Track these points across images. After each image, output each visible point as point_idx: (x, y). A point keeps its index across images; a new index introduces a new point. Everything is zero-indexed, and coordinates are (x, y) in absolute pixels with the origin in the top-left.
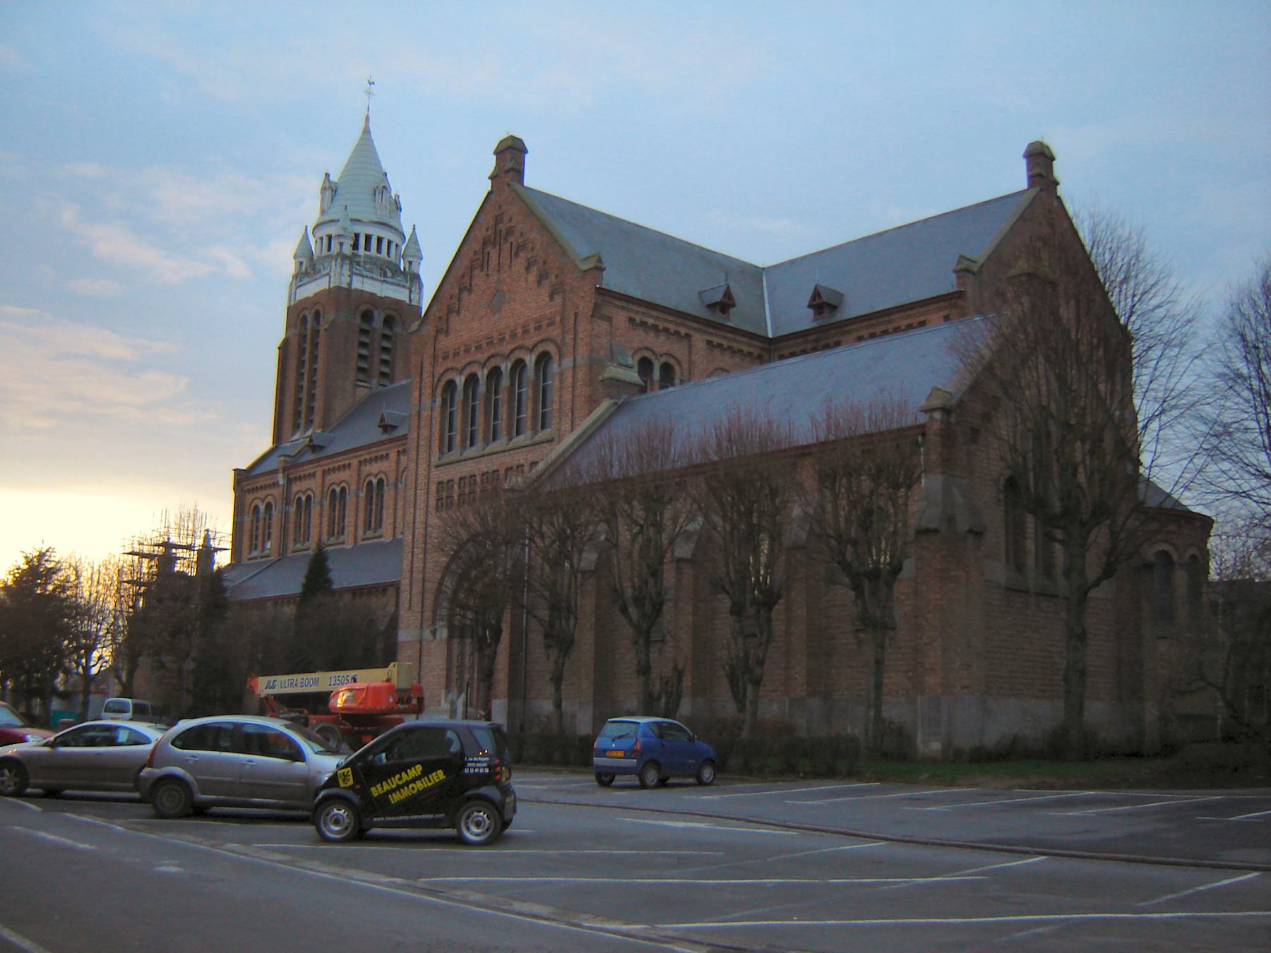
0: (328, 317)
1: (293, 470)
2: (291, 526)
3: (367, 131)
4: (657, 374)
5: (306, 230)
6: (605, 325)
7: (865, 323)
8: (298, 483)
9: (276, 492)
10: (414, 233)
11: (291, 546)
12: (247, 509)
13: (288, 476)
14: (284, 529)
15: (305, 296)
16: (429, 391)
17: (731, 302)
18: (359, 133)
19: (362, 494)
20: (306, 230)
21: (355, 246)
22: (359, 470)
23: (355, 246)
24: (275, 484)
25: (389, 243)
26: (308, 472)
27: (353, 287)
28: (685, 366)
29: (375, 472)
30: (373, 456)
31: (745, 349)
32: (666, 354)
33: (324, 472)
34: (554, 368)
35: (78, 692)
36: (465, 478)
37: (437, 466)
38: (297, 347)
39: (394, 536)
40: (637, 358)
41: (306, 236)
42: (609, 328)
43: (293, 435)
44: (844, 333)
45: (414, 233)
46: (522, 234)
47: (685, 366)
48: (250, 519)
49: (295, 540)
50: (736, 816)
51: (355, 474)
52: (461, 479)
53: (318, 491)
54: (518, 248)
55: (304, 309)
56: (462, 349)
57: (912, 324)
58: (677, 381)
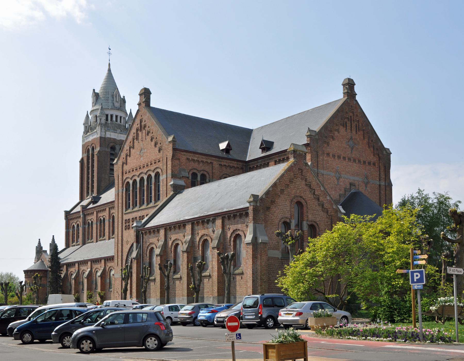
1: (86, 211)
3: (109, 70)
4: (199, 178)
5: (87, 113)
6: (177, 162)
7: (277, 155)
16: (121, 186)
17: (231, 148)
18: (106, 72)
20: (87, 113)
21: (107, 119)
23: (107, 119)
24: (80, 217)
25: (121, 117)
26: (91, 212)
27: (106, 137)
28: (211, 174)
31: (236, 166)
32: (203, 170)
34: (161, 178)
36: (141, 216)
37: (125, 214)
40: (191, 173)
41: (87, 116)
42: (179, 163)
43: (87, 197)
44: (270, 159)
46: (149, 127)
47: (211, 174)
50: (332, 349)
52: (139, 217)
53: (95, 219)
54: (148, 132)
55: (88, 146)
56: (131, 170)
58: (207, 180)
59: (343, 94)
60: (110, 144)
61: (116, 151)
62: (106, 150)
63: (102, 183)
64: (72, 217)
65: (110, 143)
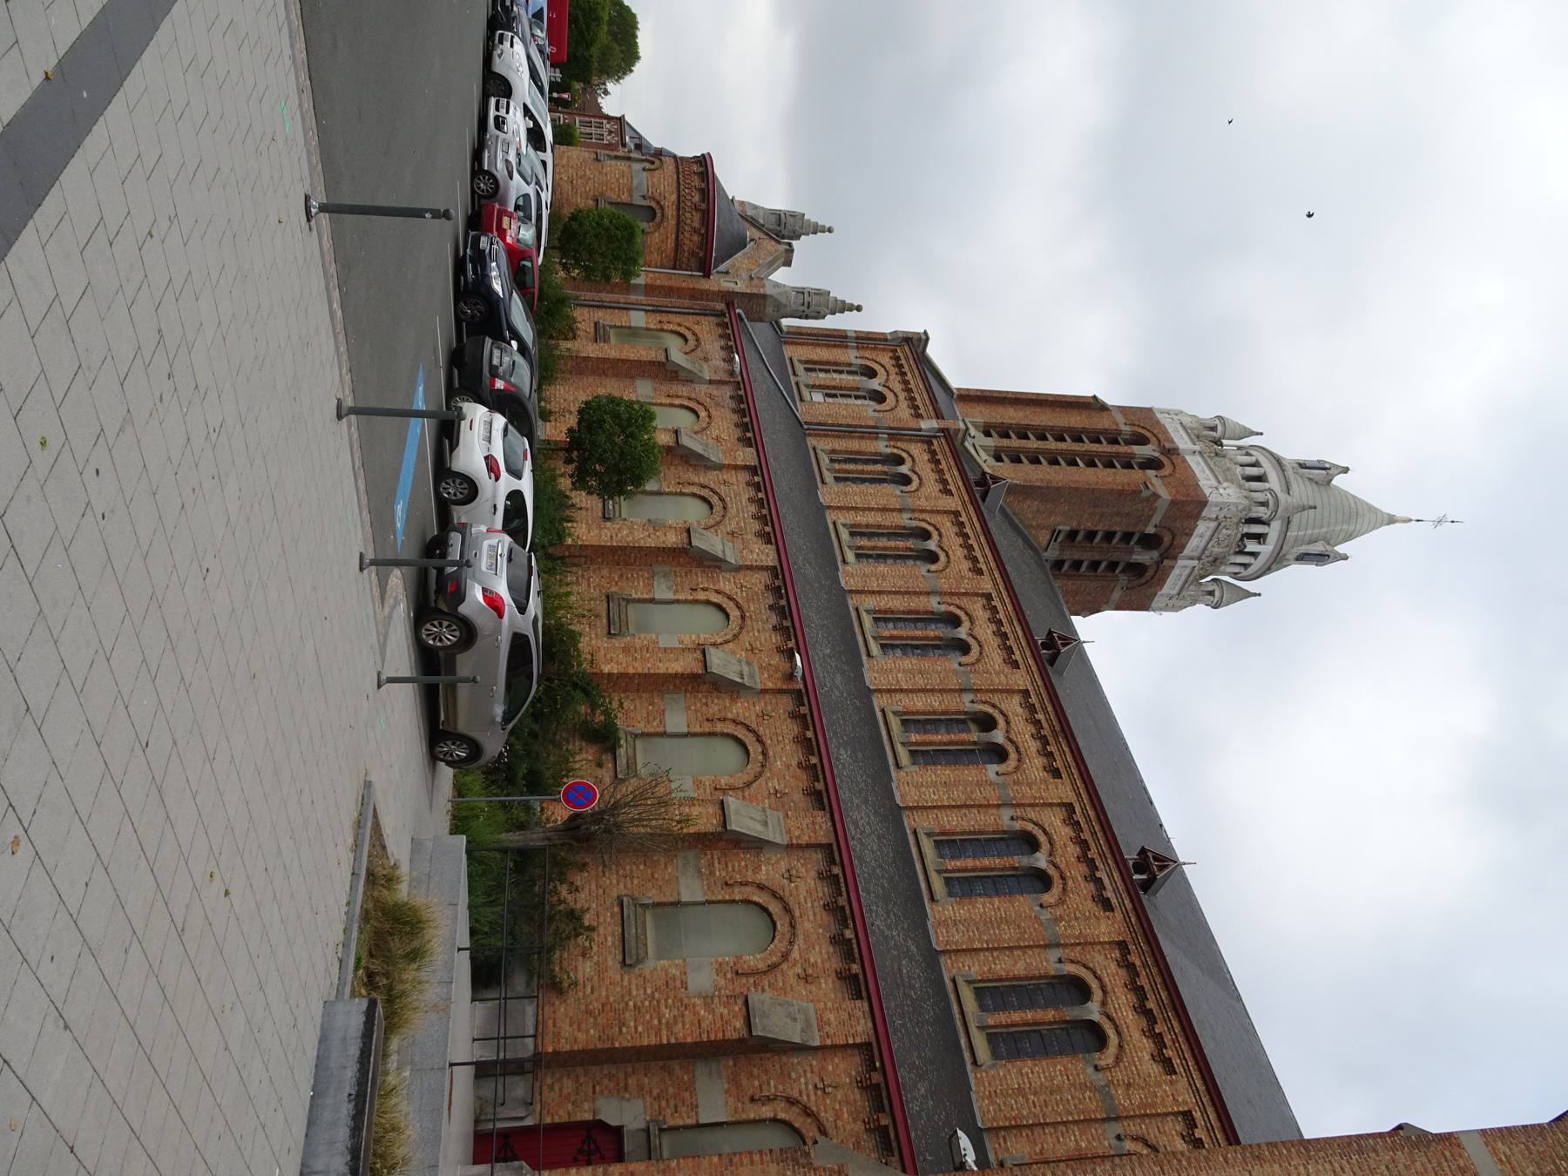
0: (1155, 481)
2: (854, 445)
3: (1392, 520)
8: (926, 457)
9: (904, 412)
10: (1248, 594)
11: (824, 444)
12: (867, 354)
13: (935, 437)
14: (848, 431)
19: (934, 604)
22: (1010, 691)
29: (978, 631)
30: (1007, 628)
33: (956, 514)
38: (1100, 426)
39: (875, 691)
45: (1248, 594)
48: (854, 361)
49: (834, 451)
51: (1000, 681)
59: (641, 54)
60: (1168, 533)
61: (1138, 549)
62: (1157, 519)
63: (1036, 503)
64: (906, 366)
65: (1173, 534)
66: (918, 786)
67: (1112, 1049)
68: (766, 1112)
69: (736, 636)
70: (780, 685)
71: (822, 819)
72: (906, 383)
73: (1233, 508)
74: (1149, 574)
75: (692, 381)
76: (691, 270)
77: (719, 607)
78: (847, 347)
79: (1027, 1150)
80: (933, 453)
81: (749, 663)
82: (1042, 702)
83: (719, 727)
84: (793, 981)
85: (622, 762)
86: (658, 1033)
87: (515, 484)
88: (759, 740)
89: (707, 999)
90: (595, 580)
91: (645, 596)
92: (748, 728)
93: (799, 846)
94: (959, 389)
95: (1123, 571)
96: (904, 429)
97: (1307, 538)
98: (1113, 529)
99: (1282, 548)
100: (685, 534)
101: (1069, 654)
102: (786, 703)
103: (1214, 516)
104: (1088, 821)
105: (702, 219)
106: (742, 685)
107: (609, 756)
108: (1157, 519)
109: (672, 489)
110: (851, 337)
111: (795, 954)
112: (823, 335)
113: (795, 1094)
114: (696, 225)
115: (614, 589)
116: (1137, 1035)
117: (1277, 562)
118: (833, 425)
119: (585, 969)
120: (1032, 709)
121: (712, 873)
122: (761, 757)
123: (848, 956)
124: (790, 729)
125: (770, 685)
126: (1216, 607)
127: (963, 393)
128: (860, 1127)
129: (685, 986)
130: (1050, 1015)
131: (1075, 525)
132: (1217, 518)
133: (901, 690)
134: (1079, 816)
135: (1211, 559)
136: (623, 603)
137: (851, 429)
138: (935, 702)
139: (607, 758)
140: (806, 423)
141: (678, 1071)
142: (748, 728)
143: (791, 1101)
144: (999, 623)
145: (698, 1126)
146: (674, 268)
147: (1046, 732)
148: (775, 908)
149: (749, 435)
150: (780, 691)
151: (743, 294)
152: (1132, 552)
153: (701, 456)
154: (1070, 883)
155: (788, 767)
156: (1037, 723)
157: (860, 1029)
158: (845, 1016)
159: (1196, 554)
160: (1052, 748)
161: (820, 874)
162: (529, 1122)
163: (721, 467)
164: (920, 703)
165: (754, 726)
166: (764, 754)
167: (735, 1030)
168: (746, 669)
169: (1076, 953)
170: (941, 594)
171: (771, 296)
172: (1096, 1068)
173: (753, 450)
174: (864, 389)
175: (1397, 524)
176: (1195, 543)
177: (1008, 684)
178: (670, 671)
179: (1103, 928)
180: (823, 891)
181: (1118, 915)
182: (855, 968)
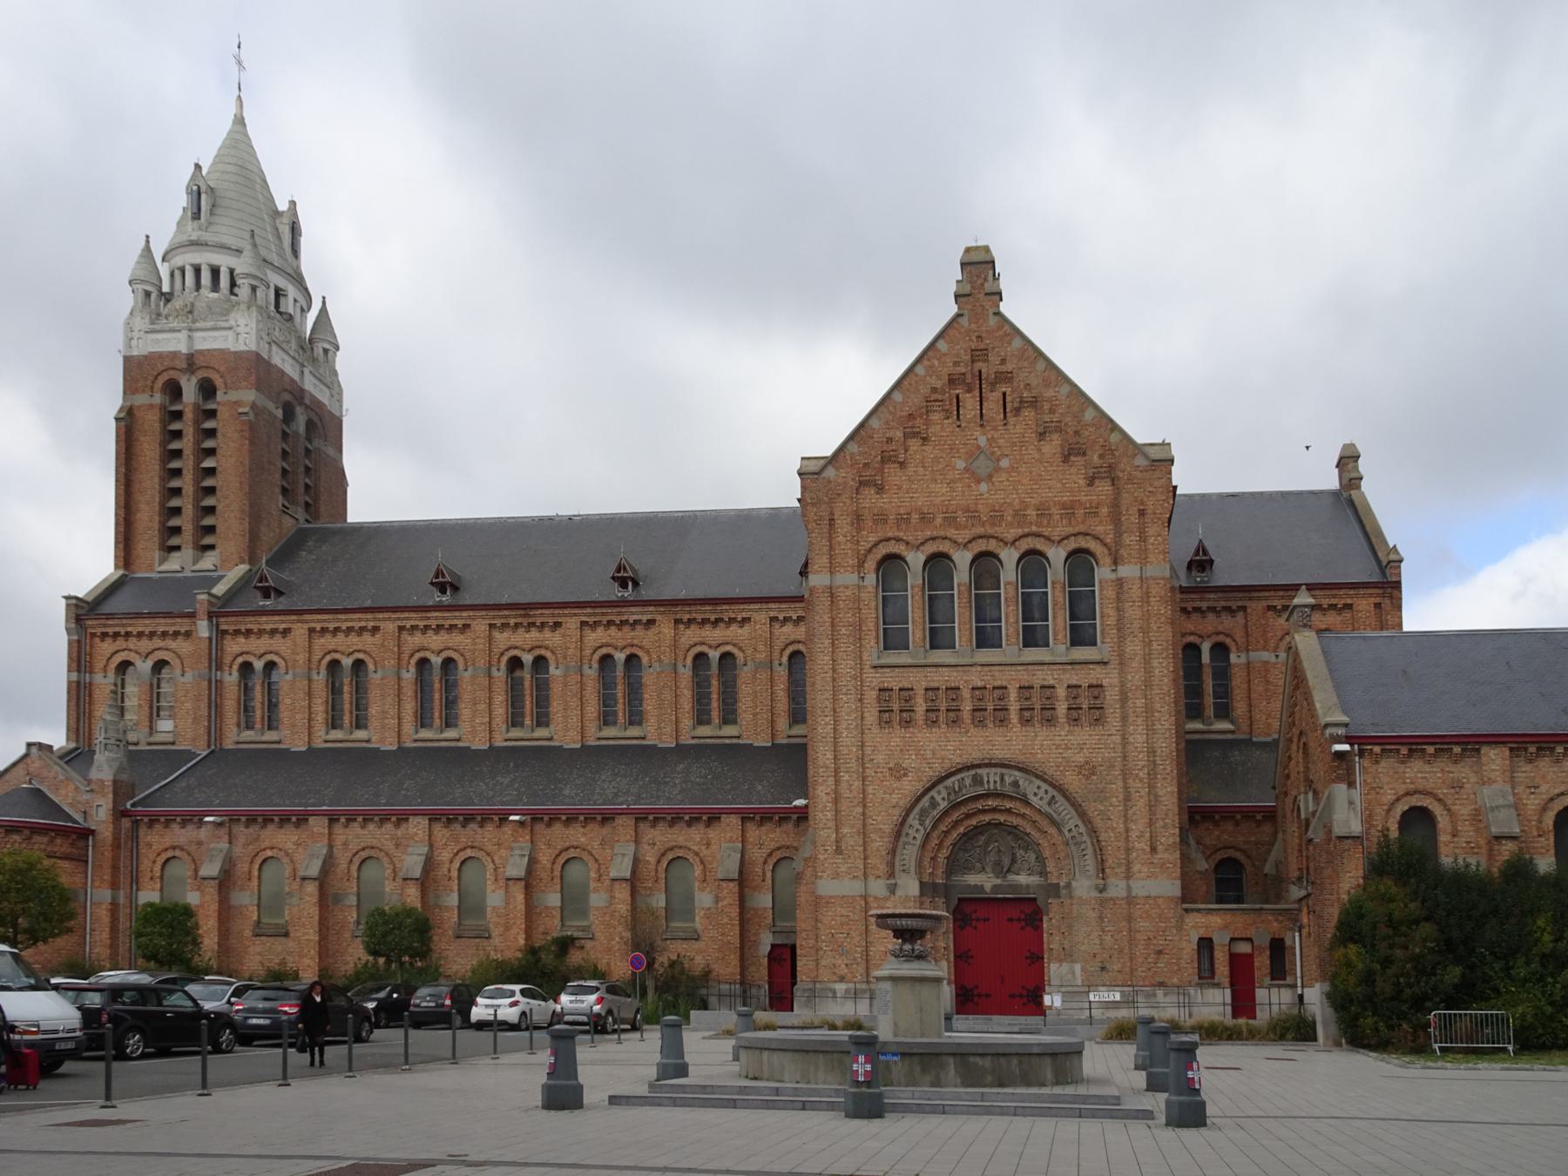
3: (240, 121)
13: (217, 625)
15: (172, 349)
18: (227, 124)
22: (490, 639)
34: (1103, 573)
35: (1043, 873)
45: (324, 311)
51: (482, 644)
57: (1336, 605)
62: (271, 406)
66: (567, 729)
67: (735, 651)
68: (769, 874)
69: (488, 854)
70: (528, 831)
71: (620, 820)
72: (140, 635)
73: (261, 325)
74: (315, 419)
75: (231, 858)
76: (88, 846)
77: (463, 863)
78: (90, 684)
79: (783, 720)
80: (237, 632)
81: (512, 849)
82: (501, 617)
83: (557, 873)
84: (709, 852)
85: (580, 934)
86: (733, 925)
87: (518, 993)
88: (567, 849)
89: (717, 899)
90: (443, 946)
91: (456, 912)
92: (558, 855)
93: (636, 836)
94: (117, 567)
95: (311, 442)
96: (210, 653)
97: (277, 242)
98: (280, 451)
99: (289, 274)
100: (409, 882)
101: (452, 573)
102: (539, 827)
103: (267, 346)
104: (594, 614)
105: (40, 834)
106: (530, 855)
107: (576, 941)
108: (271, 406)
109: (355, 885)
110: (79, 677)
111: (696, 848)
112: (78, 706)
113: (762, 859)
114: (45, 839)
115: (450, 933)
116: (728, 632)
117: (298, 280)
118: (209, 721)
119: (699, 959)
120: (505, 626)
121: (650, 888)
122: (578, 850)
123: (698, 819)
124: (558, 828)
125: (528, 837)
126: (337, 348)
127: (122, 564)
128: (778, 829)
129: (709, 909)
130: (714, 682)
131: (278, 490)
132: (269, 343)
133: (490, 723)
134: (591, 620)
135: (301, 351)
136: (461, 927)
137: (213, 704)
138: (500, 698)
139: (577, 943)
140: (209, 746)
141: (749, 916)
142: (558, 855)
143: (765, 862)
144: (427, 627)
145: (773, 908)
146: (87, 862)
147: (525, 621)
148: (670, 856)
149: (294, 819)
150: (532, 831)
151: (115, 802)
152: (296, 433)
153: (324, 862)
154: (635, 642)
155: (584, 834)
156: (517, 625)
157: (735, 821)
158: (728, 828)
159: (297, 367)
160: (538, 621)
161: (652, 827)
162: (767, 987)
163: (331, 847)
164: (500, 711)
165: (557, 852)
166: (576, 848)
167: (734, 886)
168: (516, 852)
169: (681, 654)
170: (399, 666)
171: (115, 775)
172: (745, 665)
173: (311, 820)
174: (151, 679)
175: (245, 115)
176: (290, 368)
177: (484, 638)
178: (523, 901)
179: (666, 631)
180: (662, 826)
181: (658, 617)
182: (705, 817)
